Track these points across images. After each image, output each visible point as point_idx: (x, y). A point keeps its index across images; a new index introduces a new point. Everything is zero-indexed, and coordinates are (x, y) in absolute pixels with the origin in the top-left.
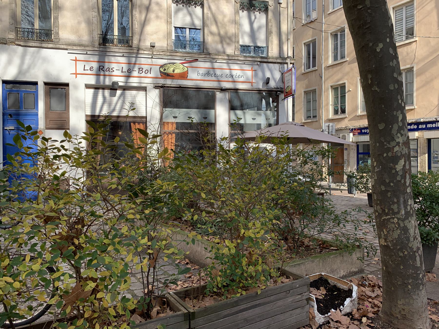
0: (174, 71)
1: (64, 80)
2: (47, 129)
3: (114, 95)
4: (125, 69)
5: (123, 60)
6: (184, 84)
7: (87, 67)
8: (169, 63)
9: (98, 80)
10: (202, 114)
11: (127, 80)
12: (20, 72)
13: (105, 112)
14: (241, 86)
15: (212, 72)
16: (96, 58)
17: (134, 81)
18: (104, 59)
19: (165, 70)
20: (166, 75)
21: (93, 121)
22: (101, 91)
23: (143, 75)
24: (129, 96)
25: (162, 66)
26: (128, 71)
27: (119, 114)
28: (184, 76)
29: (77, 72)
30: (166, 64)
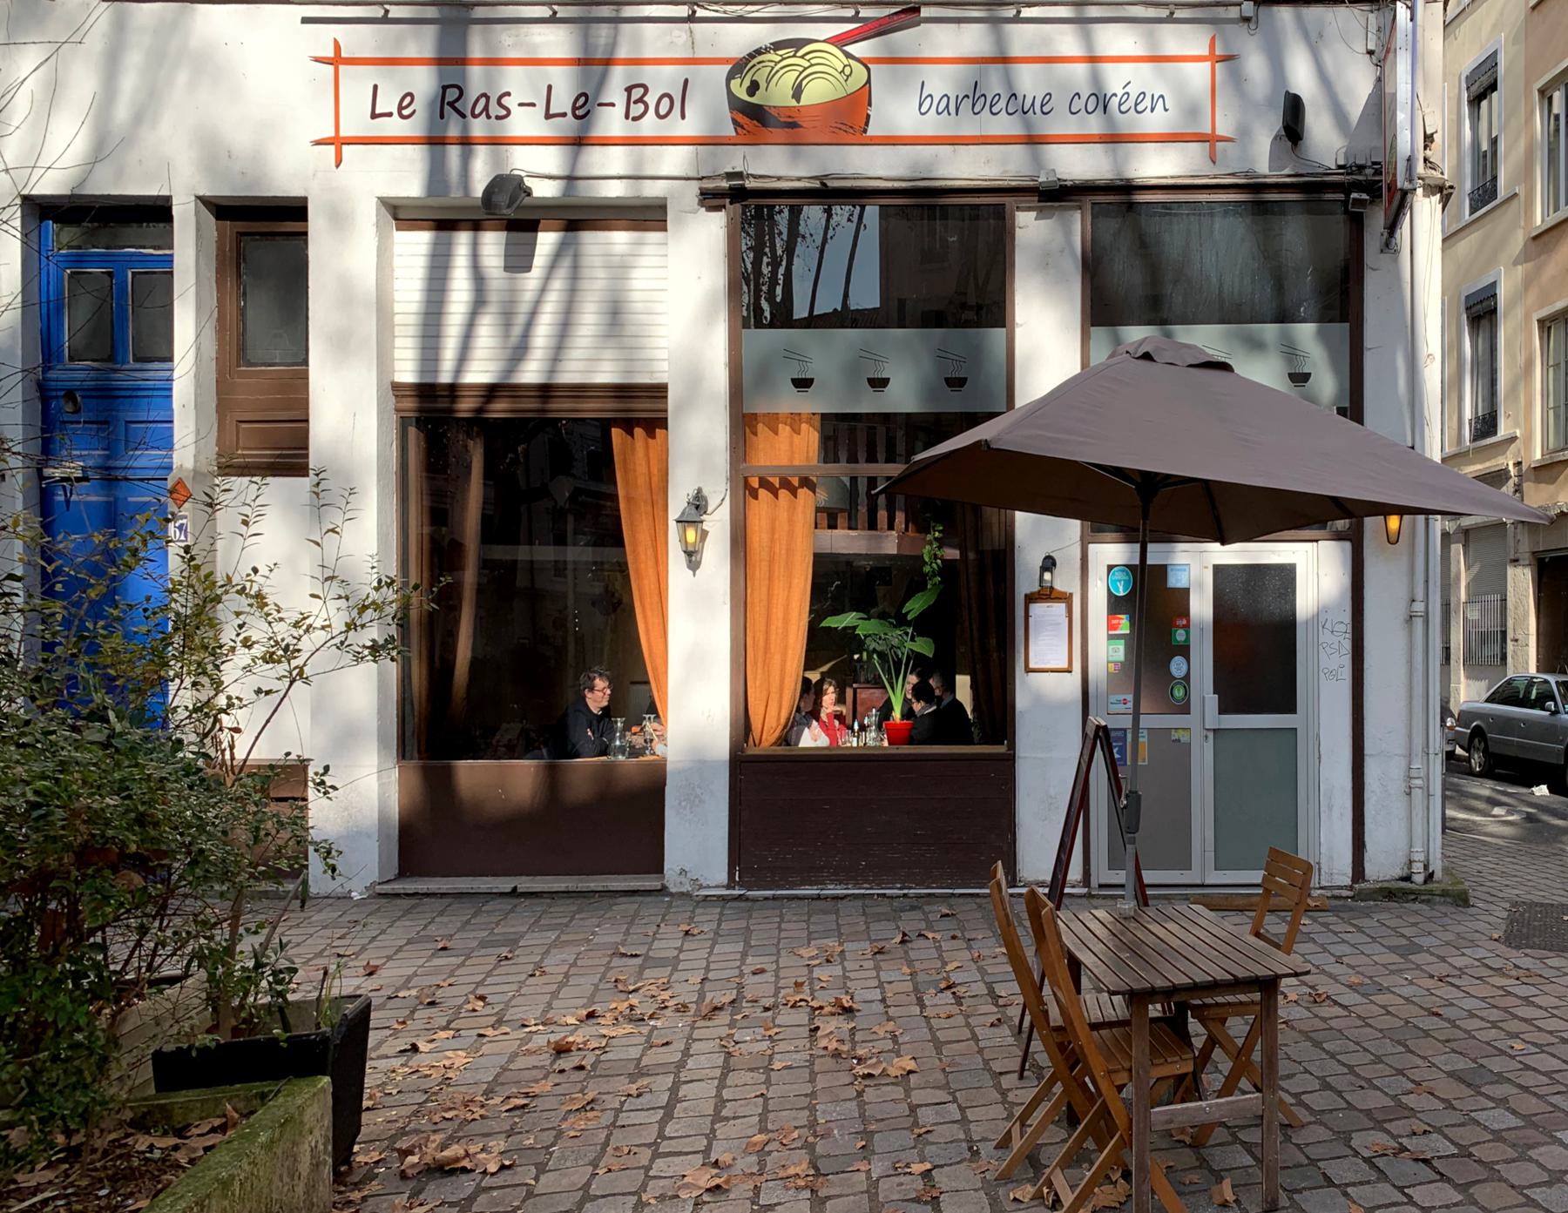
0: (797, 93)
1: (283, 183)
2: (230, 467)
3: (518, 261)
4: (563, 102)
5: (554, 41)
6: (849, 171)
7: (387, 103)
8: (777, 46)
9: (436, 175)
10: (941, 356)
11: (574, 161)
12: (102, 149)
13: (480, 373)
14: (1156, 165)
15: (994, 83)
16: (422, 43)
17: (609, 173)
18: (464, 44)
19: (754, 88)
20: (754, 119)
21: (434, 420)
22: (463, 239)
23: (649, 126)
24: (598, 261)
25: (739, 67)
26: (574, 108)
27: (552, 371)
28: (849, 118)
29: (343, 133)
30: (759, 52)
